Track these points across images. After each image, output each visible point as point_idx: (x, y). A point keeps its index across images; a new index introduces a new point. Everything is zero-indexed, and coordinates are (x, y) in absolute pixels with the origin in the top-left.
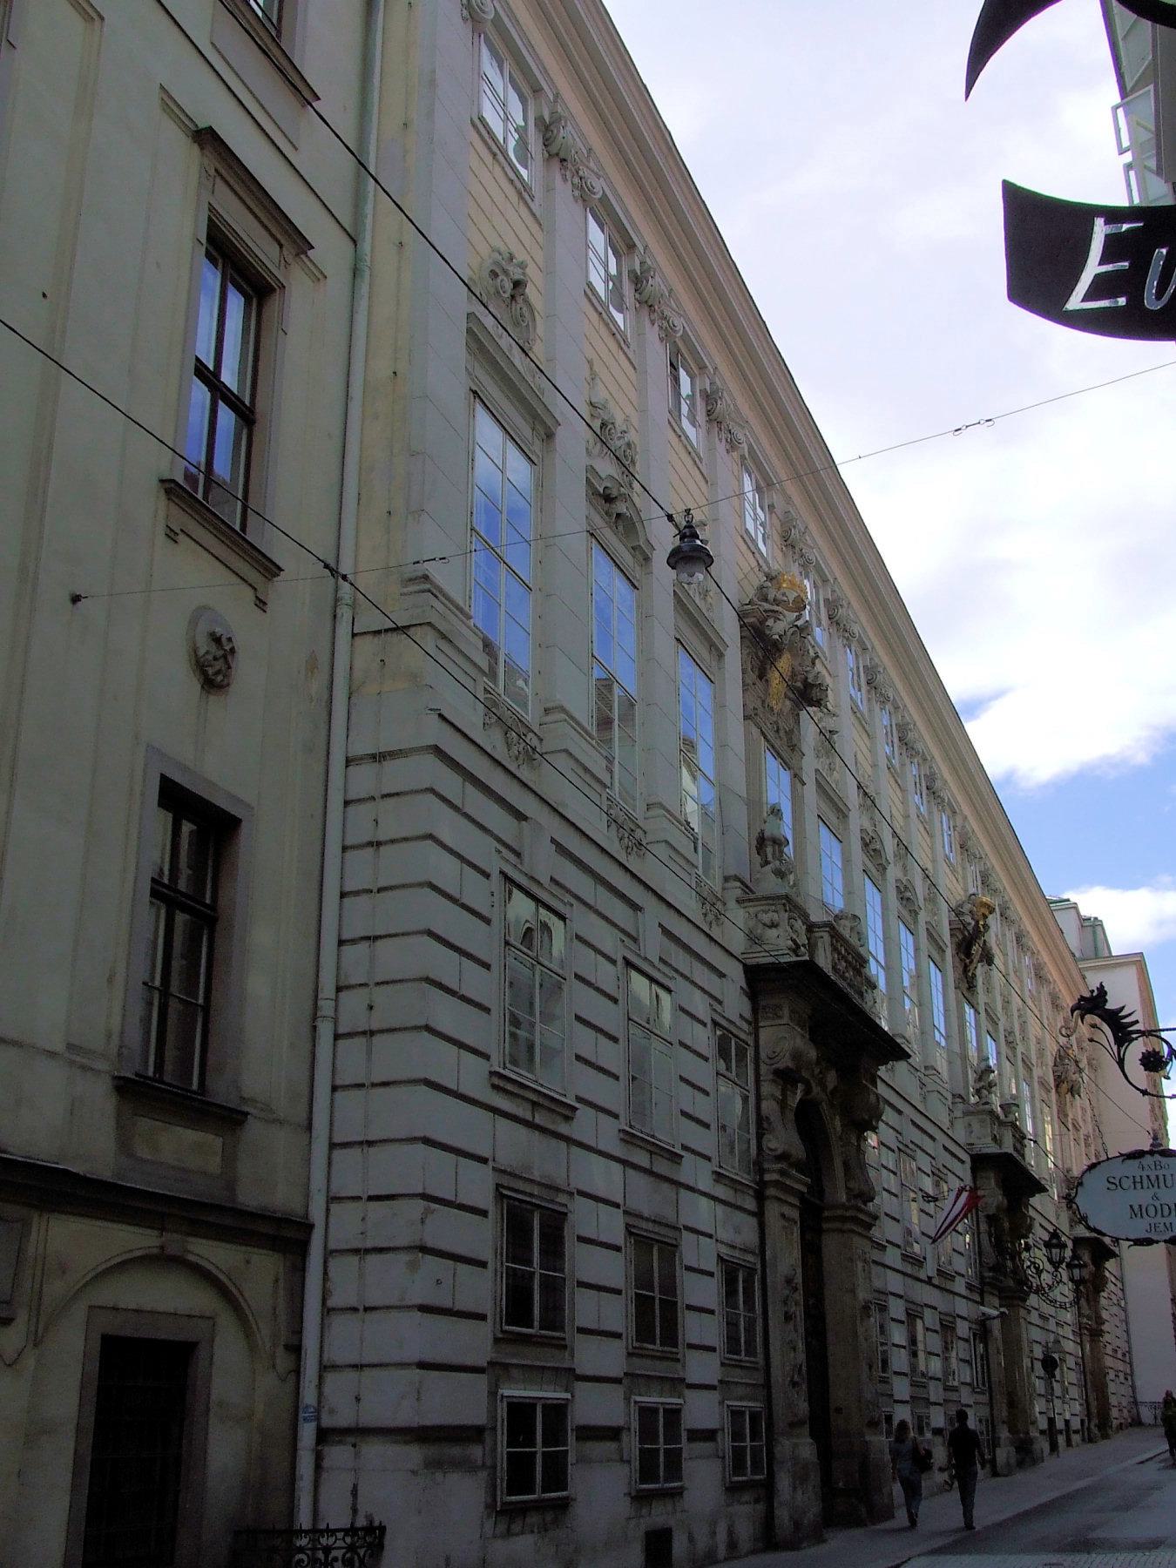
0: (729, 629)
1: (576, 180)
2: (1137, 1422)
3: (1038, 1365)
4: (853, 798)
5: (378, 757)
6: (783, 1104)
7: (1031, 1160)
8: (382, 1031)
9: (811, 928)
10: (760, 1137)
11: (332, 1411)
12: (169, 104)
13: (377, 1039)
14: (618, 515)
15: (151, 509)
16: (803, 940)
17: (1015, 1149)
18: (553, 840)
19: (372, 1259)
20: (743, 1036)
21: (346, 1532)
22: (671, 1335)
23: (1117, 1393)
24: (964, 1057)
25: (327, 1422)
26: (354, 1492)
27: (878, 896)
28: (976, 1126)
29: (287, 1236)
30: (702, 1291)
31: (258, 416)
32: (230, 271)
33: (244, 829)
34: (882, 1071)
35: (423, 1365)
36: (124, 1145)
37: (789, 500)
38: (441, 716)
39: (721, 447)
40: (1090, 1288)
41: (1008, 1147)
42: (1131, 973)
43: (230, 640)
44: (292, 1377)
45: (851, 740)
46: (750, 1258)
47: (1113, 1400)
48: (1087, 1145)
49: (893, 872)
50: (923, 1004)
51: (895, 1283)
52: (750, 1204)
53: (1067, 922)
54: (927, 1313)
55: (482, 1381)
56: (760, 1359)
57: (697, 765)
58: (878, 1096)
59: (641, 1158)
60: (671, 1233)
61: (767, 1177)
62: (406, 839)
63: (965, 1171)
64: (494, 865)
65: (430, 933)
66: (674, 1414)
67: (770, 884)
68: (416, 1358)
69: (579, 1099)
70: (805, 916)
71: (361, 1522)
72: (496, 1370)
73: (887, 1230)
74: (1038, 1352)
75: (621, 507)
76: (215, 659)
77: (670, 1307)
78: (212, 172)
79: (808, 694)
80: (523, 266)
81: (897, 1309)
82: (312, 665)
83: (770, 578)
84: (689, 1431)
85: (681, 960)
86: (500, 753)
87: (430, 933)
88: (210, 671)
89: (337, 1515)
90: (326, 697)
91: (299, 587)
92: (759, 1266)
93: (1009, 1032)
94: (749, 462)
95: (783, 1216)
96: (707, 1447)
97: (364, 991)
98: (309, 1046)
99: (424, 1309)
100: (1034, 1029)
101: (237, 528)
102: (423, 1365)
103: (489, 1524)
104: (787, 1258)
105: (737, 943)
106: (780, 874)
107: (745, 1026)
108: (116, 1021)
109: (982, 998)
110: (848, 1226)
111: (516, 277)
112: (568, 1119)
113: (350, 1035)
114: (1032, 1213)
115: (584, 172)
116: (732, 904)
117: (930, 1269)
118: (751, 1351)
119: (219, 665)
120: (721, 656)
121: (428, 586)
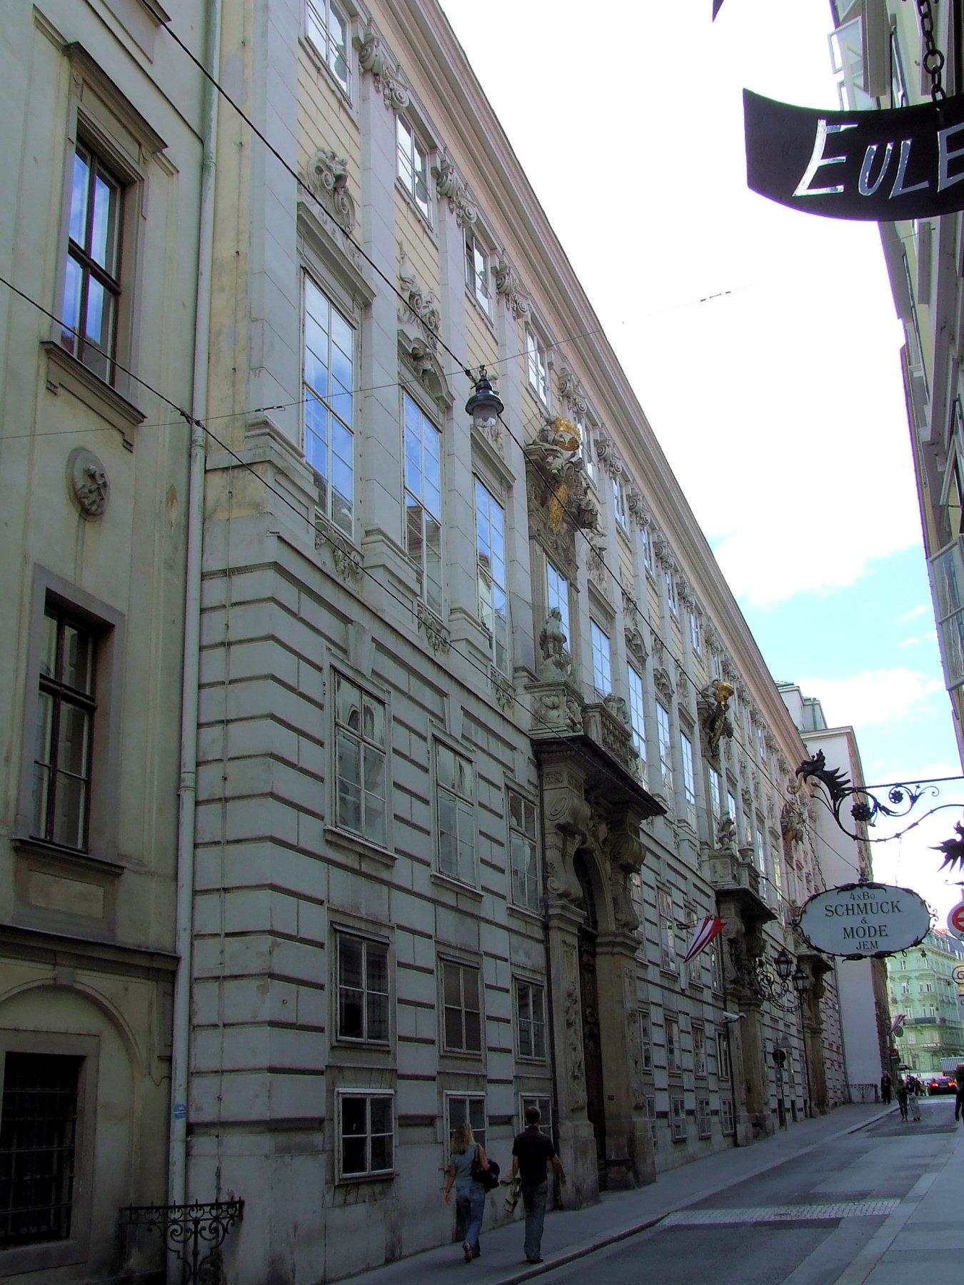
0: (516, 464)
1: (387, 92)
2: (848, 1101)
3: (770, 1058)
4: (618, 603)
5: (228, 573)
6: (563, 853)
7: (763, 893)
8: (234, 798)
9: (585, 708)
10: (545, 879)
11: (199, 1109)
12: (42, 23)
13: (230, 805)
14: (425, 371)
15: (32, 366)
16: (578, 718)
17: (751, 885)
18: (373, 640)
19: (229, 985)
20: (530, 798)
21: (212, 1206)
22: (475, 1040)
23: (832, 1078)
24: (709, 812)
25: (194, 1118)
26: (218, 1175)
27: (639, 682)
28: (719, 867)
29: (159, 968)
30: (500, 1004)
31: (123, 289)
32: (97, 166)
33: (117, 630)
34: (644, 824)
35: (273, 1070)
36: (22, 895)
37: (564, 358)
38: (279, 537)
39: (509, 315)
40: (812, 995)
41: (745, 883)
42: (844, 740)
43: (102, 475)
44: (166, 1081)
45: (615, 555)
46: (539, 977)
47: (829, 1084)
48: (808, 882)
49: (651, 663)
50: (676, 770)
51: (655, 994)
52: (539, 934)
53: (791, 701)
54: (681, 1018)
55: (321, 1082)
56: (547, 1058)
57: (491, 568)
58: (640, 844)
59: (449, 898)
60: (473, 958)
61: (551, 911)
62: (251, 640)
63: (710, 904)
64: (428, 731)
65: (273, 717)
66: (477, 1104)
67: (552, 674)
68: (266, 1063)
69: (397, 851)
70: (580, 699)
71: (224, 1198)
72: (333, 1071)
73: (651, 953)
74: (770, 1047)
75: (427, 365)
76: (90, 492)
77: (473, 1017)
78: (80, 81)
79: (582, 518)
80: (343, 163)
81: (657, 1015)
82: (172, 496)
83: (549, 422)
84: (491, 1118)
85: (480, 737)
86: (329, 568)
87: (273, 717)
88: (86, 502)
89: (204, 1193)
90: (183, 521)
91: (160, 431)
92: (545, 984)
93: (746, 792)
94: (532, 327)
95: (564, 942)
96: (503, 1130)
97: (221, 765)
98: (174, 811)
99: (273, 1024)
100: (765, 788)
101: (107, 382)
102: (273, 1070)
103: (328, 1198)
104: (567, 976)
105: (525, 721)
106: (560, 665)
107: (531, 789)
108: (13, 793)
109: (723, 764)
110: (617, 950)
111: (338, 173)
112: (389, 867)
113: (208, 801)
114: (764, 936)
115: (393, 84)
116: (520, 690)
117: (683, 983)
118: (539, 1052)
119: (94, 496)
120: (510, 487)
121: (267, 430)
